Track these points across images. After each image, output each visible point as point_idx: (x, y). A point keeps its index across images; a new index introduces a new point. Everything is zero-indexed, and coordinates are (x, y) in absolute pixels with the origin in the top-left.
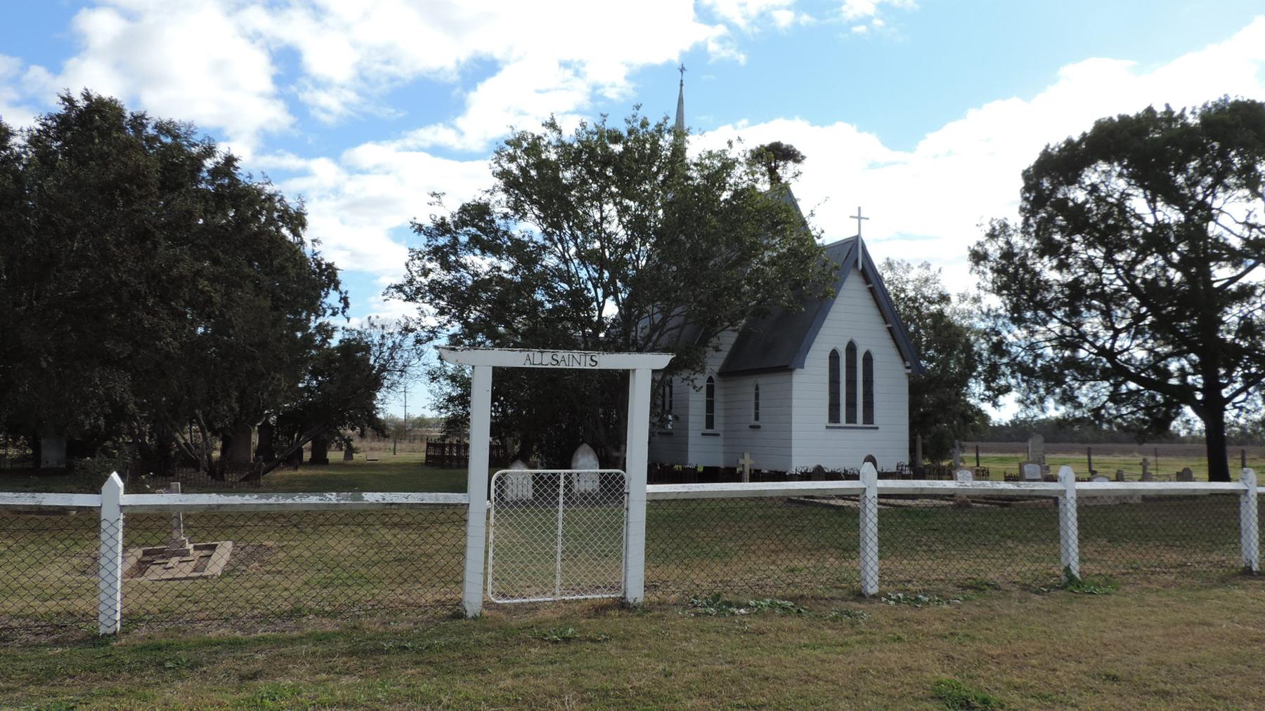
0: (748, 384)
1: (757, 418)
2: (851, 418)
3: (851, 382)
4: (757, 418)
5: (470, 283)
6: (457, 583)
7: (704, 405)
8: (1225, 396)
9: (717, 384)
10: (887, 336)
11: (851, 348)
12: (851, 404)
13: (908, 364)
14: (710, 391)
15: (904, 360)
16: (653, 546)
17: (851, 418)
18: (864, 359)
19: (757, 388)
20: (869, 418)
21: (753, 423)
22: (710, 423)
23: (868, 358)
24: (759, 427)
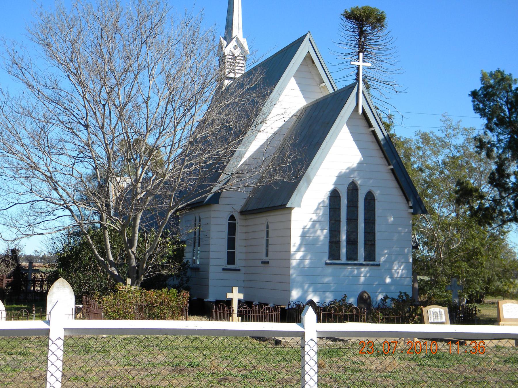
0: (261, 220)
1: (267, 255)
2: (352, 255)
3: (352, 220)
4: (267, 255)
5: (474, 194)
6: (383, 319)
7: (225, 242)
8: (513, 342)
9: (239, 221)
10: (390, 177)
11: (353, 189)
12: (352, 242)
13: (411, 205)
14: (232, 229)
15: (408, 200)
16: (416, 319)
17: (352, 255)
18: (366, 199)
19: (268, 227)
20: (370, 255)
21: (265, 259)
22: (231, 258)
23: (370, 198)
24: (268, 263)
